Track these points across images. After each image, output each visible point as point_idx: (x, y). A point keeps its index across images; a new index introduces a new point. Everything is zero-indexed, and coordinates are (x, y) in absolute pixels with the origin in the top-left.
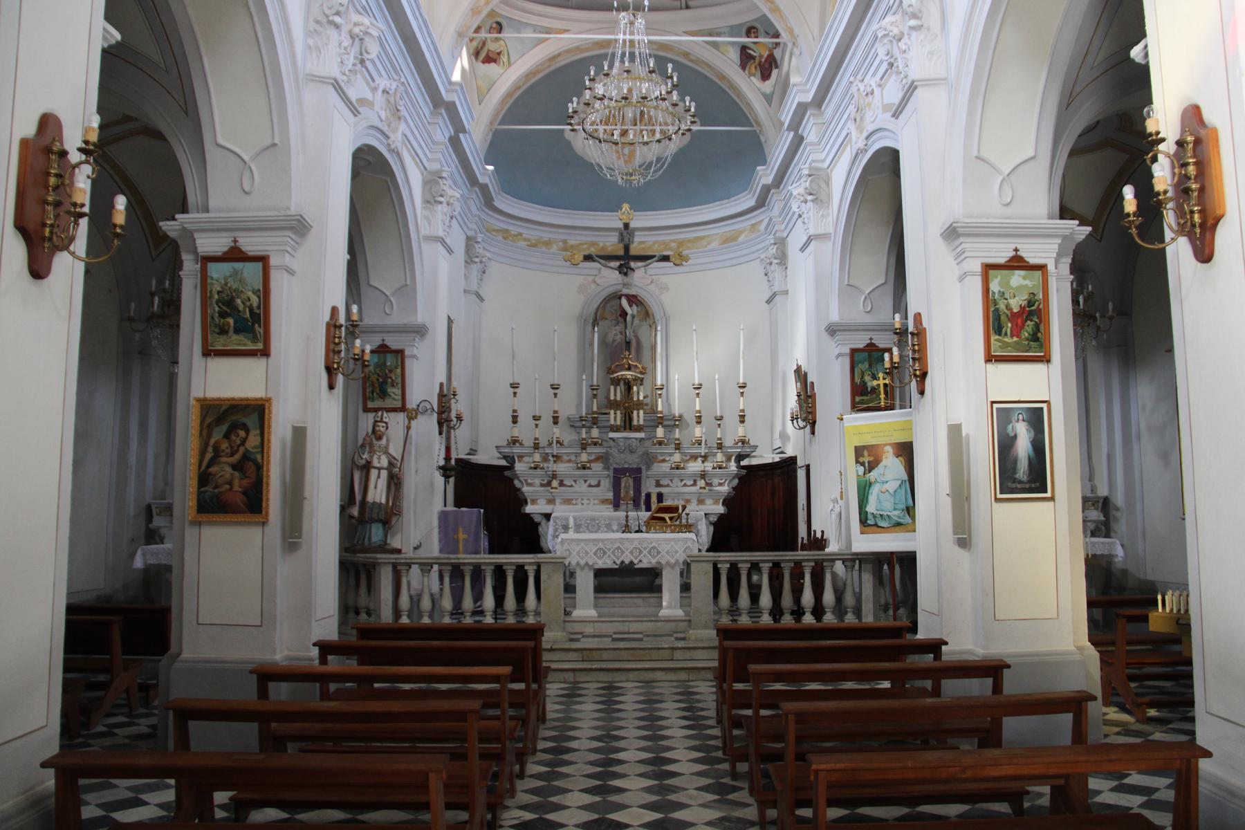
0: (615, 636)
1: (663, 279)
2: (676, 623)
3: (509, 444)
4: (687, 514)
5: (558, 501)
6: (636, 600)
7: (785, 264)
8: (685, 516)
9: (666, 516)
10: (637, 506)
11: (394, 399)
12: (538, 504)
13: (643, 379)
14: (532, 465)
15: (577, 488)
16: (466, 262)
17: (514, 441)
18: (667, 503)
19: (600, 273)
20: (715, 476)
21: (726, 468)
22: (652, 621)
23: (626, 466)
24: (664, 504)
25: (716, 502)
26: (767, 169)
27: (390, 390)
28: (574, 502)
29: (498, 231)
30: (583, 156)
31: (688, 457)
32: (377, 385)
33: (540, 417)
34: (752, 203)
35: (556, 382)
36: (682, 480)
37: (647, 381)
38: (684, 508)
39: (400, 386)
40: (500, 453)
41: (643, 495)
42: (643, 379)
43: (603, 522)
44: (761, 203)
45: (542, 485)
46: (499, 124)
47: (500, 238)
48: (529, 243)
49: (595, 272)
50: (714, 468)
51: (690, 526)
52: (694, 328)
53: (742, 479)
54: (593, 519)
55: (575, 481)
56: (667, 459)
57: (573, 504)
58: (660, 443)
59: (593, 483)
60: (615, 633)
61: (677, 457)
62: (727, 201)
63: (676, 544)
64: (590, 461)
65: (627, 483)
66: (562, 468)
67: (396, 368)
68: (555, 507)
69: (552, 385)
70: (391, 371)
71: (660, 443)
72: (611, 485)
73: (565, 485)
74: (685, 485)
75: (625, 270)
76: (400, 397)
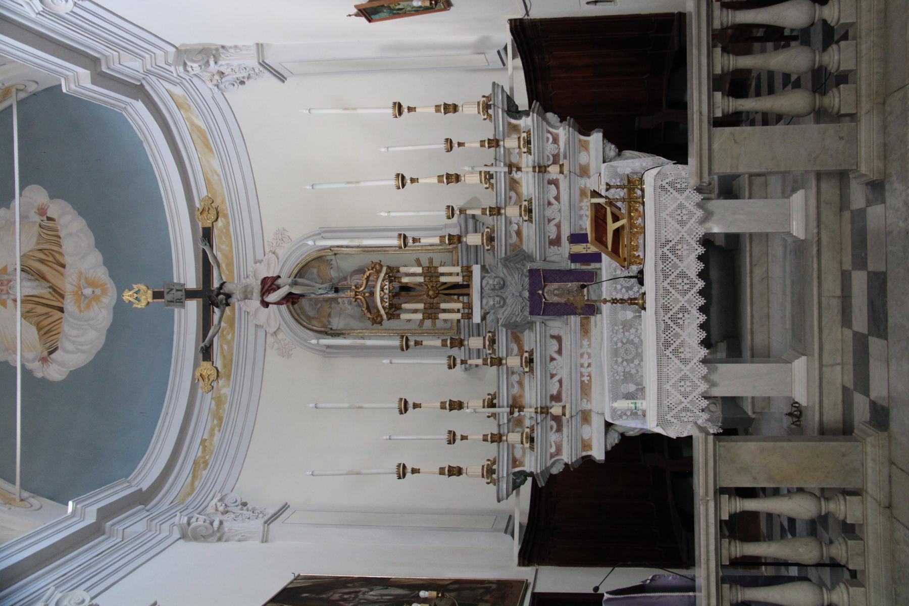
0: (860, 322)
1: (269, 236)
2: (823, 205)
3: (493, 482)
4: (609, 187)
5: (585, 406)
6: (756, 280)
7: (217, 50)
8: (612, 191)
9: (611, 227)
10: (591, 278)
12: (590, 439)
13: (389, 267)
14: (527, 445)
15: (564, 374)
16: (220, 539)
17: (489, 472)
18: (587, 225)
19: (261, 327)
20: (541, 151)
21: (528, 133)
22: (819, 251)
23: (526, 294)
24: (589, 231)
25: (585, 147)
26: (66, 78)
28: (586, 379)
29: (194, 477)
30: (95, 352)
31: (513, 194)
33: (450, 432)
34: (140, 106)
35: (396, 405)
36: (549, 204)
37: (388, 260)
38: (595, 194)
40: (508, 496)
41: (573, 266)
42: (389, 267)
43: (620, 336)
44: (138, 91)
45: (559, 430)
46: (13, 482)
47: (205, 473)
48: (217, 428)
49: (261, 333)
50: (529, 152)
51: (629, 181)
52: (309, 187)
53: (546, 108)
54: (615, 352)
55: (552, 376)
56: (515, 227)
57: (590, 381)
58: (491, 239)
59: (556, 348)
60: (846, 319)
61: (512, 212)
62: (145, 145)
63: (666, 208)
64: (521, 351)
65: (552, 293)
66: (532, 397)
68: (594, 409)
69: (401, 413)
71: (491, 239)
72: (558, 318)
73: (559, 393)
74: (557, 198)
75: (221, 297)
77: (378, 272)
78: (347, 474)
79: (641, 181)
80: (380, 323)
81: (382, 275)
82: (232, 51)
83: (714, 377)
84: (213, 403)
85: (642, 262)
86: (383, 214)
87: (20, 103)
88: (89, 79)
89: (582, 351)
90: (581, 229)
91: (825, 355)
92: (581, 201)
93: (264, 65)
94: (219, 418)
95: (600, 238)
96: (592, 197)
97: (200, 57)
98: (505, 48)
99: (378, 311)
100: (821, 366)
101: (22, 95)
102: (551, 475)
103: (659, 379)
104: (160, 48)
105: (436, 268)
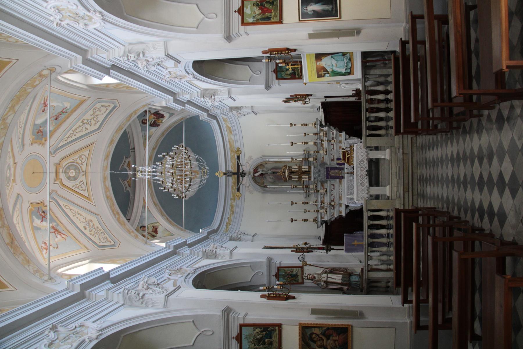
0: (398, 178)
1: (247, 158)
3: (316, 223)
4: (346, 148)
5: (340, 202)
7: (240, 107)
9: (347, 156)
10: (342, 169)
11: (298, 271)
12: (342, 211)
13: (289, 167)
14: (325, 213)
15: (335, 194)
16: (240, 241)
17: (315, 220)
19: (244, 185)
21: (326, 132)
23: (325, 173)
25: (341, 136)
27: (294, 273)
28: (341, 195)
31: (322, 147)
32: (292, 278)
33: (305, 210)
35: (290, 203)
36: (331, 150)
37: (288, 165)
38: (343, 149)
39: (292, 269)
42: (289, 167)
45: (334, 209)
46: (183, 227)
50: (326, 137)
52: (267, 145)
54: (348, 187)
55: (332, 195)
56: (322, 156)
58: (316, 159)
59: (333, 187)
61: (322, 152)
64: (324, 189)
65: (332, 173)
67: (285, 270)
70: (286, 273)
71: (316, 159)
73: (334, 199)
74: (333, 149)
76: (297, 269)
77: (286, 167)
78: (277, 221)
79: (353, 146)
80: (286, 181)
81: (287, 168)
82: (245, 108)
83: (369, 190)
84: (230, 207)
85: (354, 165)
86: (288, 152)
87: (185, 120)
88: (206, 116)
89: (340, 188)
90: (340, 157)
91: (392, 185)
92: (340, 149)
93: (253, 112)
94: (233, 212)
95: (344, 159)
96: (343, 150)
97: (236, 109)
98: (319, 108)
99: (286, 178)
100: (392, 187)
101: (185, 119)
102: (332, 221)
103: (357, 190)
104: (225, 107)
105: (301, 167)
